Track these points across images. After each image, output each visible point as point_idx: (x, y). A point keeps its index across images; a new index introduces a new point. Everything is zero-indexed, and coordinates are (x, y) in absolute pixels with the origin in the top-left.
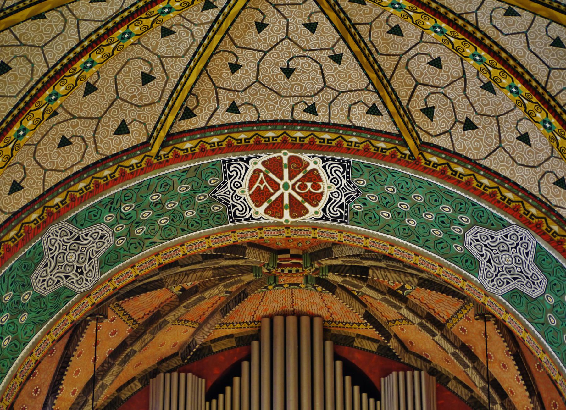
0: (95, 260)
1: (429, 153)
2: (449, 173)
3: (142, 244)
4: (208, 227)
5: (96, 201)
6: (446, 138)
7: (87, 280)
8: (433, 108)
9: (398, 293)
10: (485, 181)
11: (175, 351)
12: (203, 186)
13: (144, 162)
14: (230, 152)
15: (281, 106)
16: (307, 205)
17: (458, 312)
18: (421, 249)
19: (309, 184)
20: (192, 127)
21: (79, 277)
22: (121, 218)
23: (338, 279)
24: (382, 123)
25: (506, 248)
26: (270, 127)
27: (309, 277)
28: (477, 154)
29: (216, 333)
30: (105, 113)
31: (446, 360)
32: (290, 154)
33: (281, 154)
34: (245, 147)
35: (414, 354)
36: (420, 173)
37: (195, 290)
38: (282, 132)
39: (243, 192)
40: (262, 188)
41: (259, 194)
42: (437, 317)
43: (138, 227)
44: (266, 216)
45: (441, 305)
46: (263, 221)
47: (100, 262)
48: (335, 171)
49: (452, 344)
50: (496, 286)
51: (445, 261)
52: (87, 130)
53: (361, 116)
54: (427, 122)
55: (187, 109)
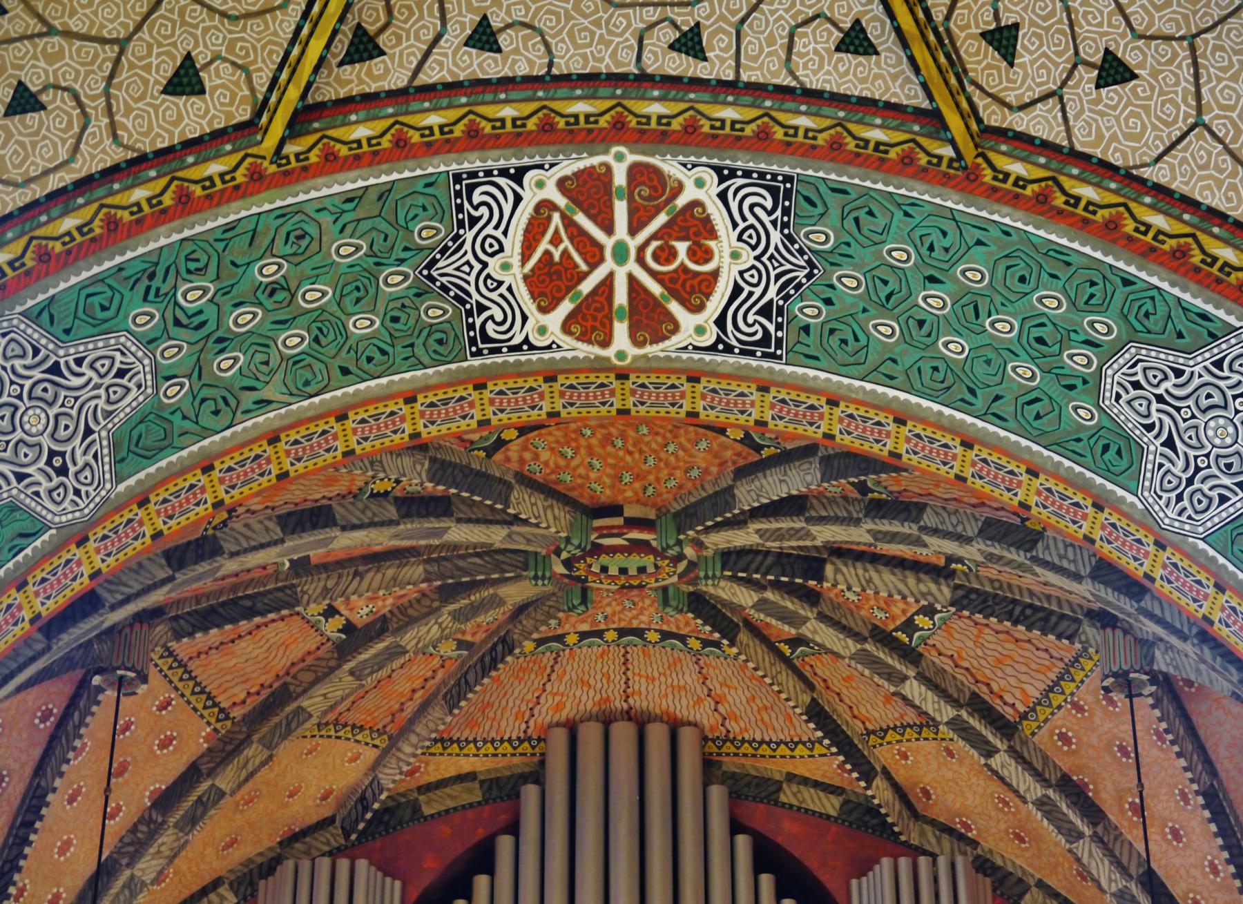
0: (102, 435)
1: (1003, 153)
2: (1059, 200)
3: (233, 402)
4: (412, 368)
5: (107, 264)
6: (1049, 111)
7: (77, 492)
8: (1016, 26)
9: (896, 639)
10: (1159, 221)
11: (326, 812)
12: (400, 245)
13: (242, 170)
14: (472, 149)
15: (610, 32)
16: (674, 307)
17: (1051, 689)
18: (980, 424)
19: (682, 247)
20: (373, 87)
21: (56, 480)
22: (177, 323)
23: (745, 598)
24: (885, 77)
25: (1217, 399)
26: (579, 92)
27: (671, 591)
28: (1134, 150)
29: (431, 768)
30: (138, 28)
31: (1017, 836)
32: (632, 158)
33: (608, 158)
34: (516, 137)
35: (933, 823)
36: (981, 200)
37: (380, 626)
38: (613, 102)
39: (506, 267)
40: (557, 257)
41: (549, 274)
42: (997, 705)
43: (222, 351)
44: (568, 339)
45: (1009, 670)
46: (558, 356)
47: (115, 445)
48: (752, 207)
49: (1038, 776)
50: (1190, 511)
51: (1046, 453)
52: (87, 74)
53: (822, 58)
54: (999, 69)
55: (359, 30)
